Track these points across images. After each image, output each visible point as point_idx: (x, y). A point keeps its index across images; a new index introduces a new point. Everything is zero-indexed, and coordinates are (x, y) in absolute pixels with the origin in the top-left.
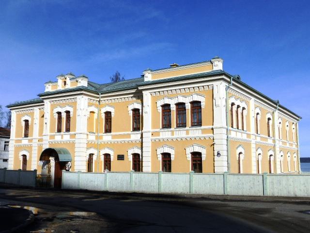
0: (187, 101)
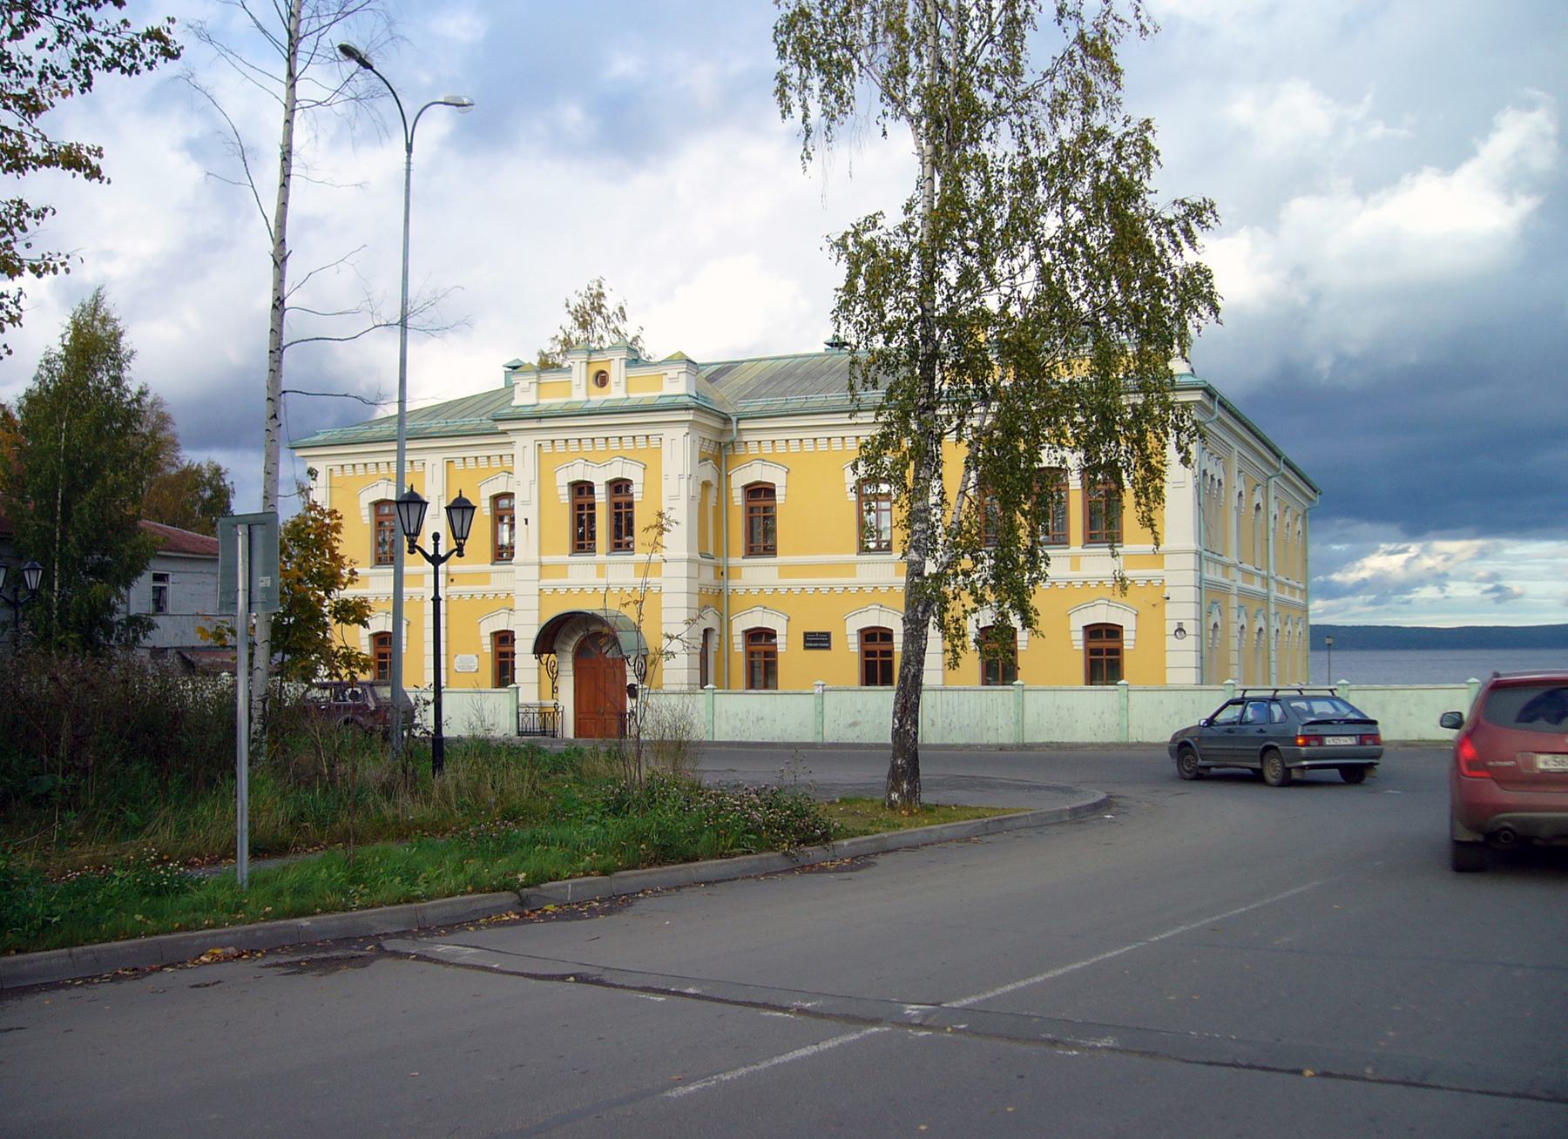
0: (600, 479)
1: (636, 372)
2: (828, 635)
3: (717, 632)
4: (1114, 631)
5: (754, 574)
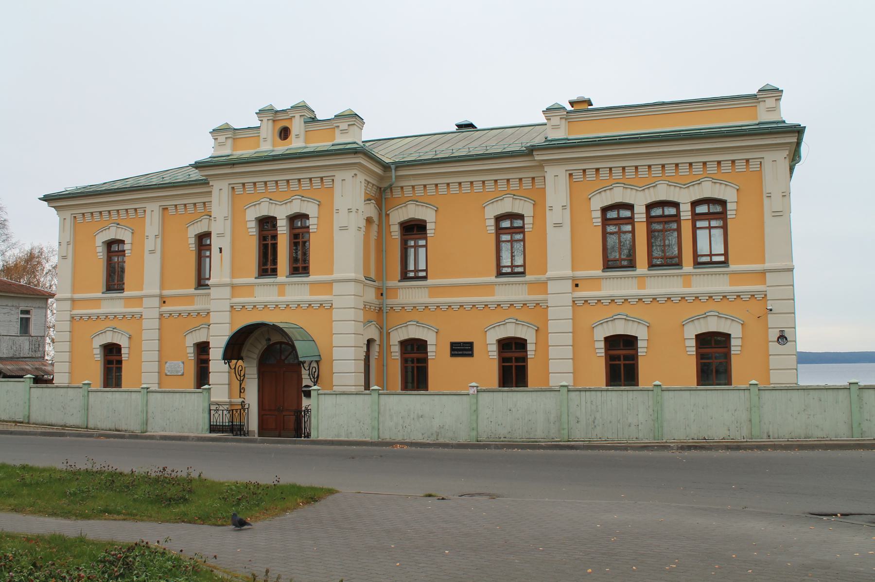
0: (281, 214)
1: (313, 127)
2: (471, 344)
3: (378, 342)
4: (630, 341)
5: (410, 295)
